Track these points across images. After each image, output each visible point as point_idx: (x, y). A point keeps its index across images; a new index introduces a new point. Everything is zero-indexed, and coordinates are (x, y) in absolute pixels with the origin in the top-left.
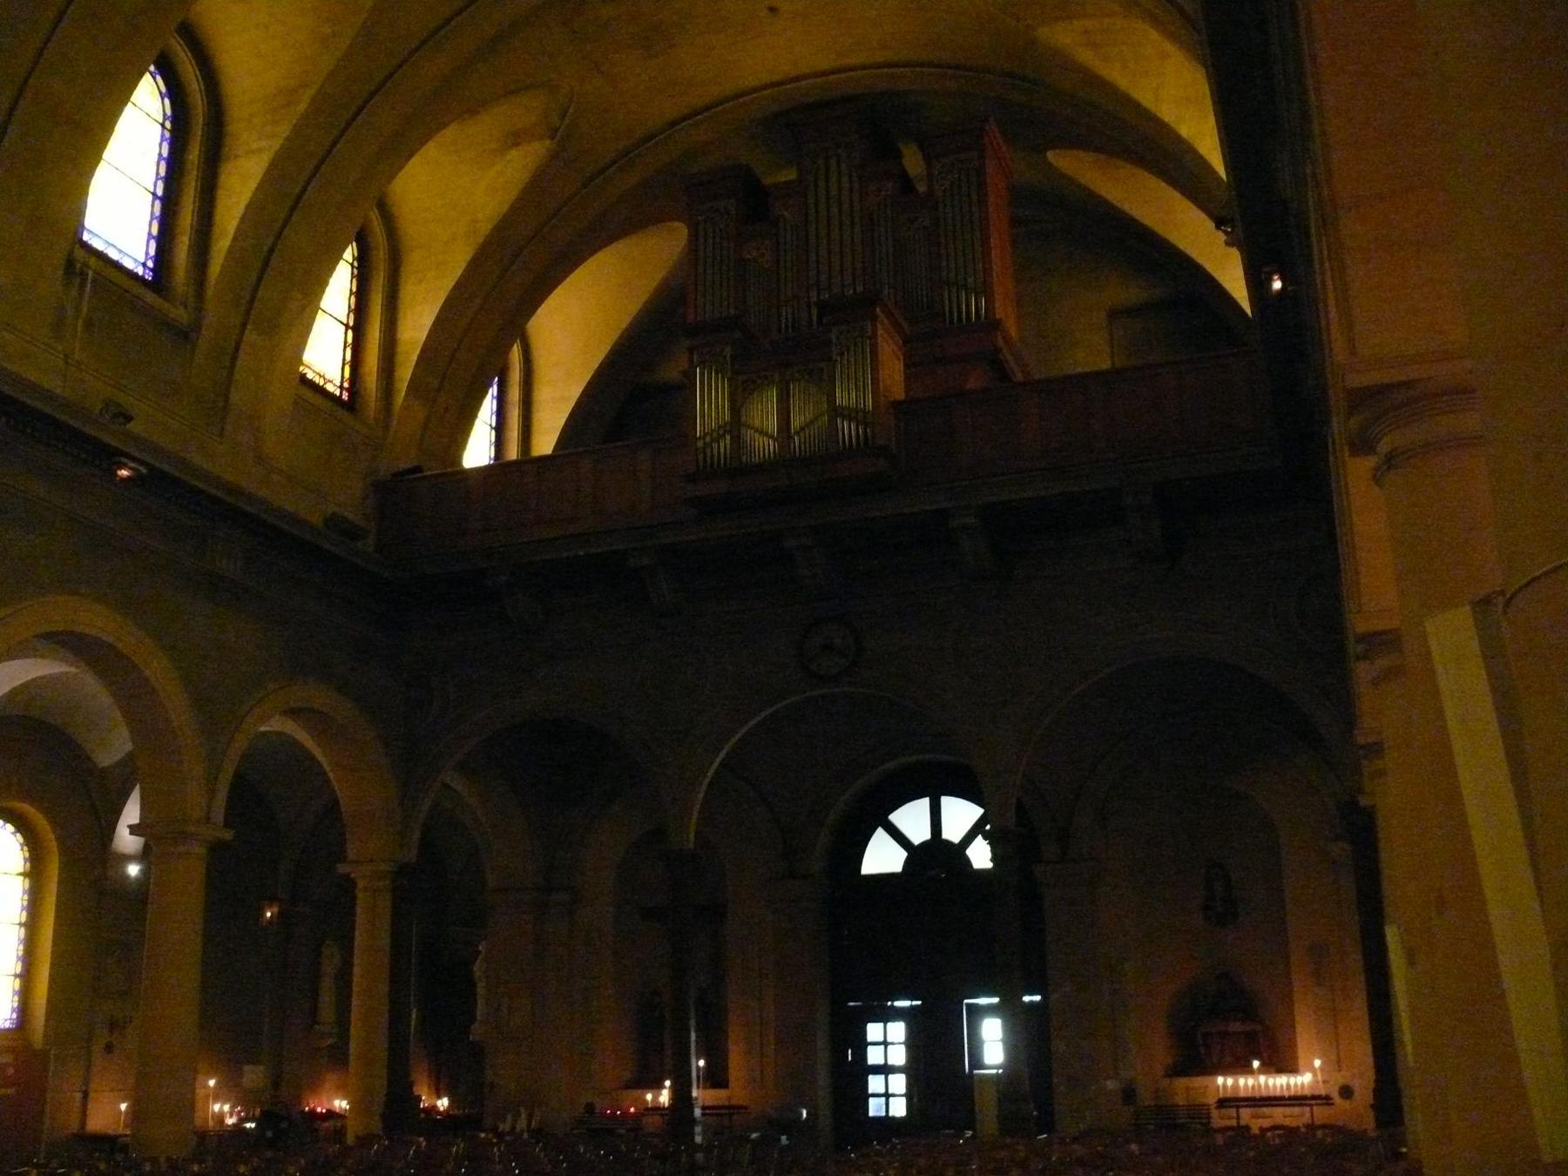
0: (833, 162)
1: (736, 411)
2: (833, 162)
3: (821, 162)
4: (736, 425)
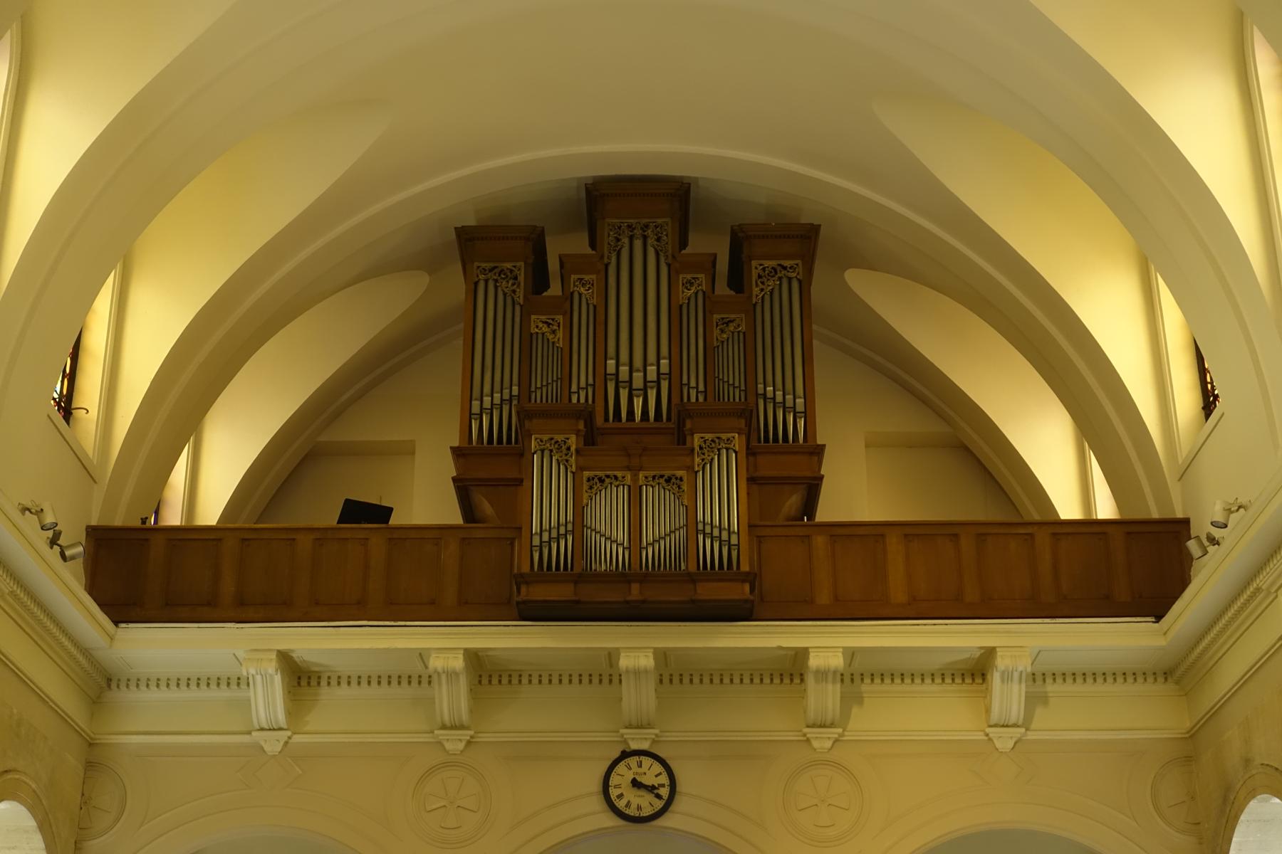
0: (638, 244)
1: (579, 510)
2: (638, 244)
3: (626, 241)
4: (579, 525)
